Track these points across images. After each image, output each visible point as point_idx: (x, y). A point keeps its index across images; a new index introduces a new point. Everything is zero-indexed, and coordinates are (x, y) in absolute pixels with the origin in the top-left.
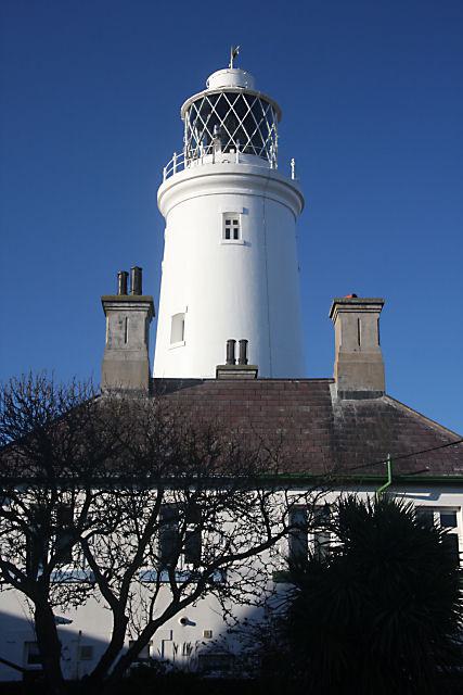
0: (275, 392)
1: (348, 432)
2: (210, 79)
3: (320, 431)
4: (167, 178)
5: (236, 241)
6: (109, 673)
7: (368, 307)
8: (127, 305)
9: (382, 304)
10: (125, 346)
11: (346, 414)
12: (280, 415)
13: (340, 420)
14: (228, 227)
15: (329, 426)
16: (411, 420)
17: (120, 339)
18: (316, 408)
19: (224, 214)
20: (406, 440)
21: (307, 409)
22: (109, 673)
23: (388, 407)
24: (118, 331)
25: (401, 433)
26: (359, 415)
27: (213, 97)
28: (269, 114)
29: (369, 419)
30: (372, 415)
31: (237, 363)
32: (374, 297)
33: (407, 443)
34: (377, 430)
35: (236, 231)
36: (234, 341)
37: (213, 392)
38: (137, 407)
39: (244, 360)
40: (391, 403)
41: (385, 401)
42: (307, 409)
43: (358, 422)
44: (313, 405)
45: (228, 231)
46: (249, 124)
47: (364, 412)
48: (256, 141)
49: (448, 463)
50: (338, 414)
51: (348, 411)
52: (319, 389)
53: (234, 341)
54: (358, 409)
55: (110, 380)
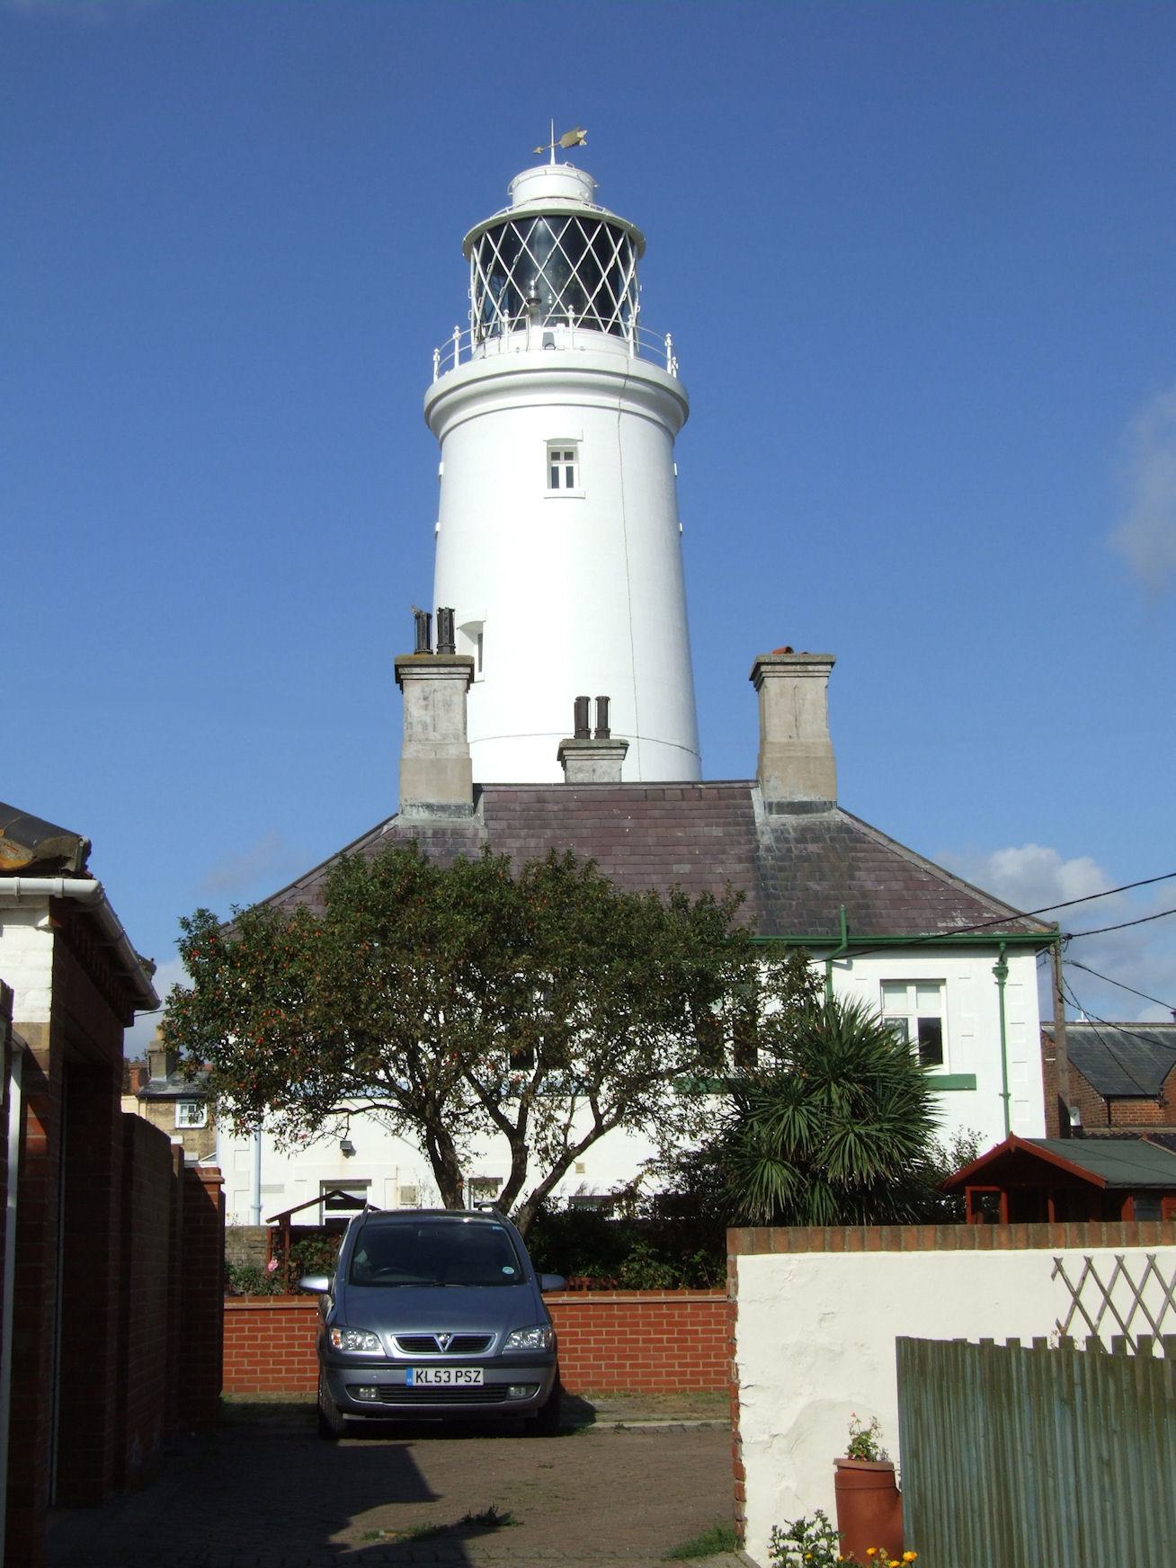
0: (667, 805)
1: (781, 869)
2: (521, 177)
3: (739, 867)
4: (441, 373)
5: (570, 492)
6: (1051, 1204)
7: (810, 668)
8: (435, 670)
9: (832, 664)
10: (432, 735)
11: (777, 840)
12: (677, 843)
13: (769, 849)
14: (555, 464)
15: (753, 858)
16: (877, 848)
17: (425, 726)
18: (731, 829)
19: (549, 442)
20: (866, 880)
21: (717, 832)
22: (1051, 1204)
23: (844, 829)
24: (422, 712)
25: (859, 869)
26: (798, 841)
27: (524, 221)
28: (623, 253)
29: (812, 848)
30: (815, 840)
31: (592, 737)
32: (817, 651)
33: (869, 885)
34: (825, 865)
35: (570, 471)
36: (588, 699)
37: (572, 805)
38: (458, 833)
39: (603, 730)
40: (847, 819)
41: (839, 817)
42: (717, 832)
43: (795, 852)
44: (729, 824)
45: (554, 473)
46: (590, 274)
47: (805, 834)
48: (605, 306)
49: (928, 913)
50: (766, 839)
51: (780, 835)
52: (734, 798)
53: (588, 699)
54: (795, 829)
55: (416, 804)
